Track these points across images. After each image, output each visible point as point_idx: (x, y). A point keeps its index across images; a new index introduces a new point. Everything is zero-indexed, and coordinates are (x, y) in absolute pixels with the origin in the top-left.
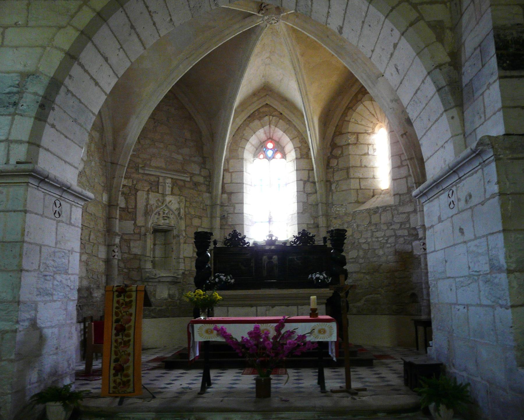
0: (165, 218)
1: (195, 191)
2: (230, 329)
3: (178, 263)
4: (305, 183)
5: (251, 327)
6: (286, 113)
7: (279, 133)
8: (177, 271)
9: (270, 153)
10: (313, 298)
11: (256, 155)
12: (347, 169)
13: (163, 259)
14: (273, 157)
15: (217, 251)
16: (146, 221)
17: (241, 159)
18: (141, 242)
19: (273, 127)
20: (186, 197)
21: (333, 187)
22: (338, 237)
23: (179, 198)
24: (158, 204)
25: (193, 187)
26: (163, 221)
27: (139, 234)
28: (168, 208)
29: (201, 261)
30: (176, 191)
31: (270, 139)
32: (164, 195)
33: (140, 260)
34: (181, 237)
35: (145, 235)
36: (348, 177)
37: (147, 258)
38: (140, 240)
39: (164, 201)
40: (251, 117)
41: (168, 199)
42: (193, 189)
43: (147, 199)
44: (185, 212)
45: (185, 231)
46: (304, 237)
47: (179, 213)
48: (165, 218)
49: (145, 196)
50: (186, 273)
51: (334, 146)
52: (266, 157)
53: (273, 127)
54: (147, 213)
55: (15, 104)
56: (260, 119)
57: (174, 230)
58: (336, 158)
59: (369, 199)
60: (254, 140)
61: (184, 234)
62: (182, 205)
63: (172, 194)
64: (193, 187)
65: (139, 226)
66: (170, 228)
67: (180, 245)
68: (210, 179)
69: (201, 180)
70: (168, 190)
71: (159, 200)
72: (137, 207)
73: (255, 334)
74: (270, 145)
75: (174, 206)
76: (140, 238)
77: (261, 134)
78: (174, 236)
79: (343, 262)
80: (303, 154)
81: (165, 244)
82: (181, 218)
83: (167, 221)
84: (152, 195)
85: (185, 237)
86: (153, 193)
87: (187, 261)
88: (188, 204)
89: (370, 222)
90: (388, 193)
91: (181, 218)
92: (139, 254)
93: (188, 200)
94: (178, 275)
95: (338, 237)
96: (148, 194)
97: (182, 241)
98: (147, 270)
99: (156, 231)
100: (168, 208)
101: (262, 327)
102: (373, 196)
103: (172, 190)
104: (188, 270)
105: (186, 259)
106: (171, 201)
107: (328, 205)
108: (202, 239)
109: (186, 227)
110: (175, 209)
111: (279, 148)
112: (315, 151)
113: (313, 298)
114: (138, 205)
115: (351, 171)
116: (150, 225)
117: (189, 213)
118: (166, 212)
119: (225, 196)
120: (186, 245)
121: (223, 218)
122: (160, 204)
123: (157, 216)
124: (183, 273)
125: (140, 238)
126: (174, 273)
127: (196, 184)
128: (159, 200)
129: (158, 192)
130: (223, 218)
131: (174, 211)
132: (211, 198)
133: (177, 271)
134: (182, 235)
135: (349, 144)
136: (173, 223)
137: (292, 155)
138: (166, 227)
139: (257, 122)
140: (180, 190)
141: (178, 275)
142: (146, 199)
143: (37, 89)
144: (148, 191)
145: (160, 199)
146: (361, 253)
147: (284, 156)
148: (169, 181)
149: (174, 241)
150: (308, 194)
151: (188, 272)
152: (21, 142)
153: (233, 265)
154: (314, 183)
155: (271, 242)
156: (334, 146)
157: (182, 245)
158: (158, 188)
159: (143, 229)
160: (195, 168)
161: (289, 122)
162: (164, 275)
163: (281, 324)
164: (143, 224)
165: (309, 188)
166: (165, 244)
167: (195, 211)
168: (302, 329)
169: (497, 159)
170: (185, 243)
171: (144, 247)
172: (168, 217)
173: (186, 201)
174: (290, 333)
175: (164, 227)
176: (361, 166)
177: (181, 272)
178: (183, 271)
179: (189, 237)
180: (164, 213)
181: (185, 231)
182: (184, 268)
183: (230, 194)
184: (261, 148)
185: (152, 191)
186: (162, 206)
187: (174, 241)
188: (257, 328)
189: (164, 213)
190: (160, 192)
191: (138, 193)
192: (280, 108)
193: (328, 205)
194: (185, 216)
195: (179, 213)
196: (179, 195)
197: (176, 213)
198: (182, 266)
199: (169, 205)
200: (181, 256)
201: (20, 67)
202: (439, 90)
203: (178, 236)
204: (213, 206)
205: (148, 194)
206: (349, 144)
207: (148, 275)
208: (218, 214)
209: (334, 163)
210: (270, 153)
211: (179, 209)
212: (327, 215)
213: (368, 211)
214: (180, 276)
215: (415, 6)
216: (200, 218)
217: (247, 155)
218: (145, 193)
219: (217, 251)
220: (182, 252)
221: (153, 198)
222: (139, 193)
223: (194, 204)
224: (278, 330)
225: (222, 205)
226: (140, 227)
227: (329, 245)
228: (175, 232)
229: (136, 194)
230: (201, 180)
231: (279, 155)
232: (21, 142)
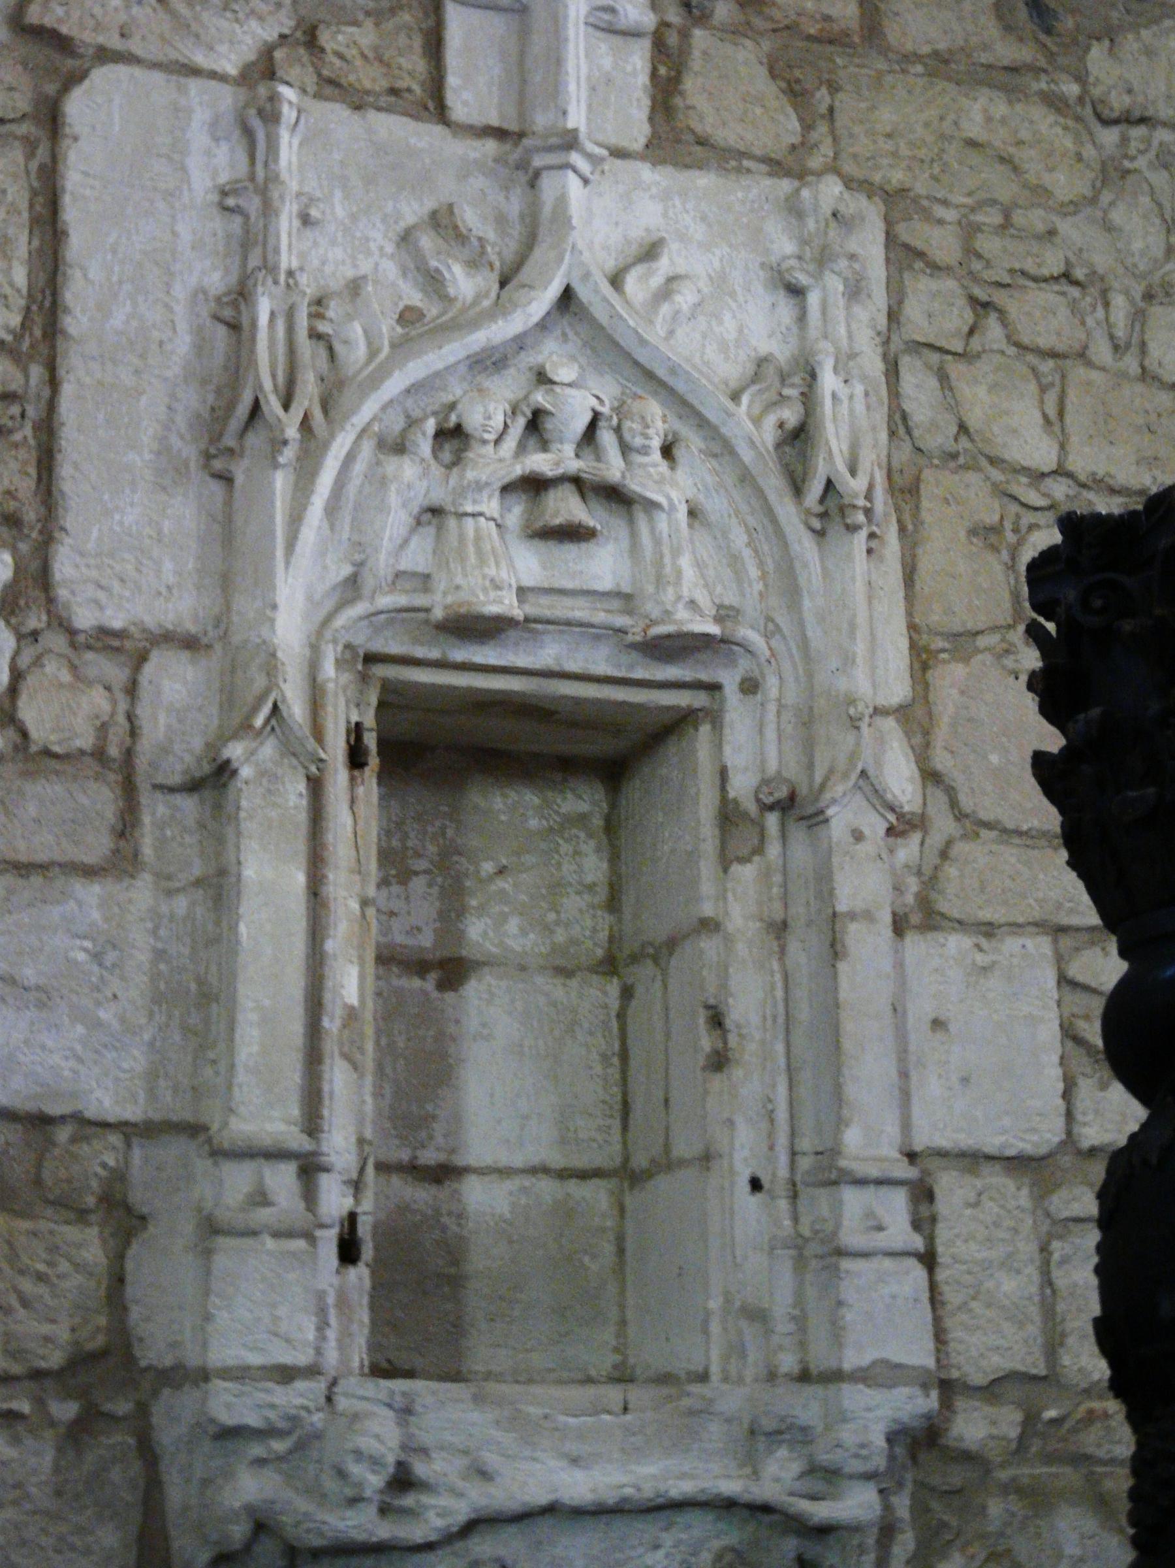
0: (567, 507)
1: (1044, 122)
8: (806, 1406)
13: (596, 1197)
16: (232, 556)
18: (141, 893)
20: (895, 200)
23: (794, 209)
24: (433, 282)
25: (1008, 51)
26: (529, 564)
27: (117, 763)
28: (608, 349)
30: (733, 86)
32: (523, 147)
33: (123, 1217)
34: (847, 814)
35: (214, 779)
37: (237, 1180)
38: (122, 861)
39: (534, 231)
41: (604, 212)
42: (1008, 79)
43: (246, 206)
44: (899, 422)
45: (916, 717)
47: (798, 438)
48: (567, 507)
49: (212, 161)
50: (973, 1427)
54: (231, 430)
57: (737, 712)
61: (900, 779)
62: (850, 328)
63: (672, 135)
64: (1008, 51)
65: (107, 639)
66: (659, 689)
67: (835, 950)
71: (443, 222)
72: (76, 322)
76: (126, 825)
78: (729, 816)
81: (609, 965)
82: (832, 512)
83: (602, 565)
84: (312, 142)
85: (902, 826)
86: (336, 116)
87: (985, 1227)
88: (936, 309)
90: (466, 1452)
91: (832, 512)
92: (104, 1102)
93: (942, 243)
94: (825, 1477)
96: (255, 124)
97: (866, 880)
98: (231, 1405)
99: (446, 744)
100: (608, 349)
103: (665, 92)
104: (992, 1390)
105: (953, 1191)
106: (650, 252)
109: (922, 660)
110: (732, 370)
114: (80, 294)
116: (293, 609)
117: (968, 450)
118: (573, 409)
120: (939, 959)
122: (464, 283)
123: (415, 477)
124: (921, 1442)
125: (126, 825)
126: (758, 1438)
128: (443, 222)
129: (434, 105)
131: (713, 406)
133: (806, 1406)
134: (868, 784)
136: (690, 595)
138: (599, 660)
140: (796, 94)
141: (825, 1477)
142: (226, 200)
144: (264, 68)
145: (471, 218)
149: (739, 899)
151: (1008, 1421)
157: (869, 944)
158: (434, 45)
159: (175, 691)
162: (578, 1486)
164: (181, 609)
166: (609, 965)
167: (1055, 422)
170: (918, 917)
171: (198, 1002)
172: (615, 496)
173: (904, 256)
175: (548, 653)
177: (870, 1418)
178: (911, 1404)
179: (973, 825)
180: (536, 425)
181: (916, 717)
182: (921, 1355)
185: (330, 86)
186: (500, 309)
187: (739, 899)
189: (536, 425)
190: (472, 92)
191: (77, 107)
194: (906, 490)
195: (798, 438)
196: (788, 166)
197: (754, 430)
198: (883, 1316)
199: (630, 308)
200: (869, 1140)
203: (795, 807)
205: (255, 124)
207: (250, 1487)
214: (856, 1504)
218: (208, 104)
220: (869, 1074)
221: (350, 201)
222: (98, 108)
223: (1044, 316)
226: (129, 649)
228: (747, 748)
229: (51, 118)
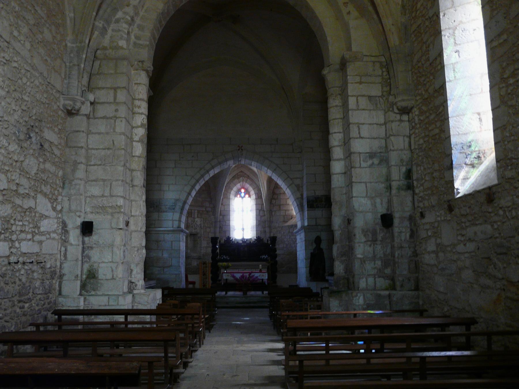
2: (235, 275)
3: (201, 250)
4: (260, 211)
5: (241, 274)
6: (251, 176)
7: (247, 186)
9: (243, 195)
10: (260, 265)
11: (236, 196)
12: (280, 206)
14: (244, 197)
15: (221, 245)
17: (229, 199)
19: (244, 183)
21: (273, 214)
22: (274, 239)
29: (214, 250)
31: (243, 188)
32: (194, 218)
36: (280, 210)
40: (234, 178)
41: (196, 220)
46: (259, 239)
51: (274, 193)
52: (241, 196)
53: (244, 183)
55: (174, 209)
56: (238, 178)
58: (275, 199)
59: (289, 220)
60: (235, 189)
62: (202, 222)
63: (198, 217)
68: (214, 208)
69: (210, 209)
70: (196, 216)
73: (242, 277)
74: (243, 191)
75: (199, 223)
77: (239, 185)
79: (275, 250)
80: (259, 197)
89: (289, 232)
95: (274, 239)
101: (245, 274)
102: (292, 218)
107: (271, 222)
108: (214, 240)
111: (247, 192)
112: (265, 195)
113: (260, 265)
115: (282, 207)
119: (221, 217)
121: (220, 227)
127: (208, 212)
130: (220, 227)
132: (215, 218)
135: (281, 194)
137: (254, 196)
139: (236, 180)
143: (180, 204)
146: (285, 246)
147: (250, 196)
148: (196, 211)
150: (261, 217)
152: (176, 220)
153: (230, 251)
154: (264, 211)
155: (243, 240)
156: (274, 193)
160: (207, 204)
161: (252, 180)
163: (250, 273)
165: (261, 212)
168: (256, 275)
169: (305, 232)
174: (253, 276)
176: (286, 204)
183: (224, 216)
184: (238, 192)
188: (243, 275)
192: (248, 173)
193: (271, 222)
201: (174, 197)
202: (298, 205)
204: (216, 222)
206: (281, 194)
208: (218, 226)
209: (274, 201)
210: (243, 195)
211: (201, 224)
212: (270, 227)
213: (289, 226)
215: (291, 179)
216: (210, 228)
217: (232, 196)
219: (221, 245)
224: (249, 275)
225: (220, 222)
227: (269, 242)
228: (199, 235)
230: (210, 209)
231: (247, 196)
232: (176, 220)
